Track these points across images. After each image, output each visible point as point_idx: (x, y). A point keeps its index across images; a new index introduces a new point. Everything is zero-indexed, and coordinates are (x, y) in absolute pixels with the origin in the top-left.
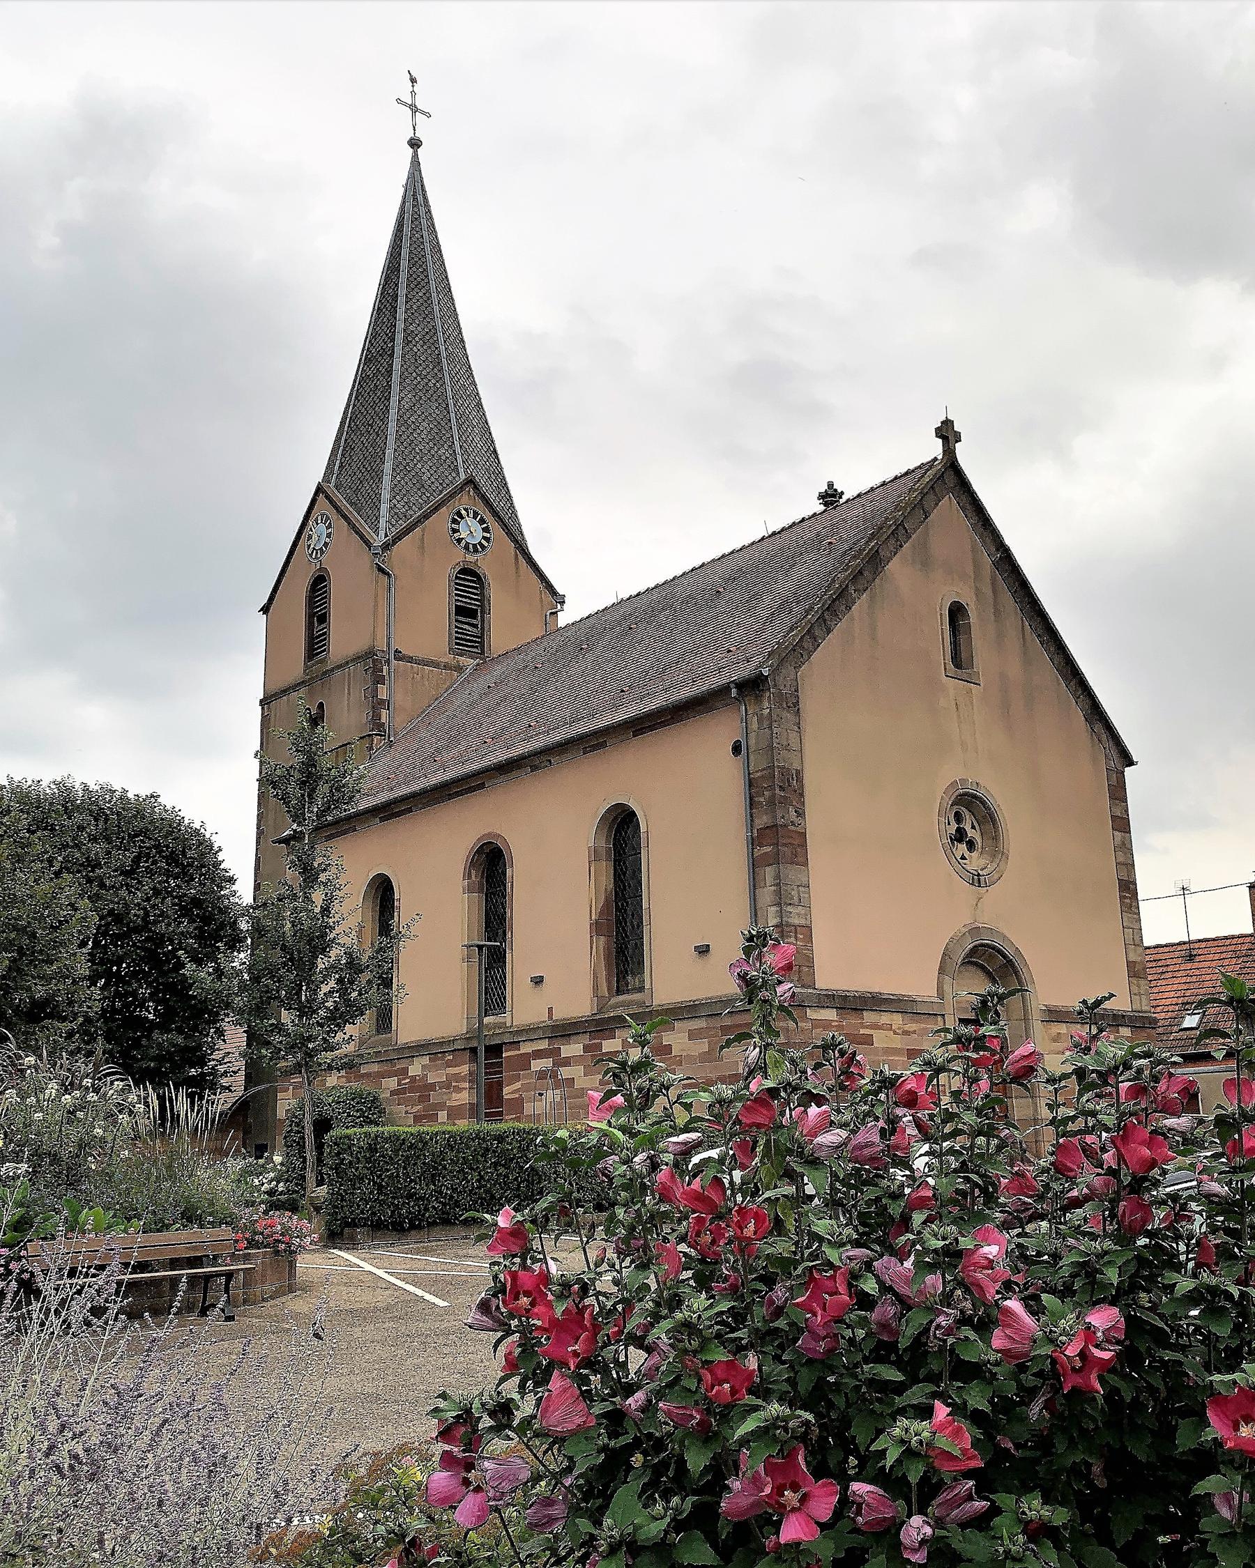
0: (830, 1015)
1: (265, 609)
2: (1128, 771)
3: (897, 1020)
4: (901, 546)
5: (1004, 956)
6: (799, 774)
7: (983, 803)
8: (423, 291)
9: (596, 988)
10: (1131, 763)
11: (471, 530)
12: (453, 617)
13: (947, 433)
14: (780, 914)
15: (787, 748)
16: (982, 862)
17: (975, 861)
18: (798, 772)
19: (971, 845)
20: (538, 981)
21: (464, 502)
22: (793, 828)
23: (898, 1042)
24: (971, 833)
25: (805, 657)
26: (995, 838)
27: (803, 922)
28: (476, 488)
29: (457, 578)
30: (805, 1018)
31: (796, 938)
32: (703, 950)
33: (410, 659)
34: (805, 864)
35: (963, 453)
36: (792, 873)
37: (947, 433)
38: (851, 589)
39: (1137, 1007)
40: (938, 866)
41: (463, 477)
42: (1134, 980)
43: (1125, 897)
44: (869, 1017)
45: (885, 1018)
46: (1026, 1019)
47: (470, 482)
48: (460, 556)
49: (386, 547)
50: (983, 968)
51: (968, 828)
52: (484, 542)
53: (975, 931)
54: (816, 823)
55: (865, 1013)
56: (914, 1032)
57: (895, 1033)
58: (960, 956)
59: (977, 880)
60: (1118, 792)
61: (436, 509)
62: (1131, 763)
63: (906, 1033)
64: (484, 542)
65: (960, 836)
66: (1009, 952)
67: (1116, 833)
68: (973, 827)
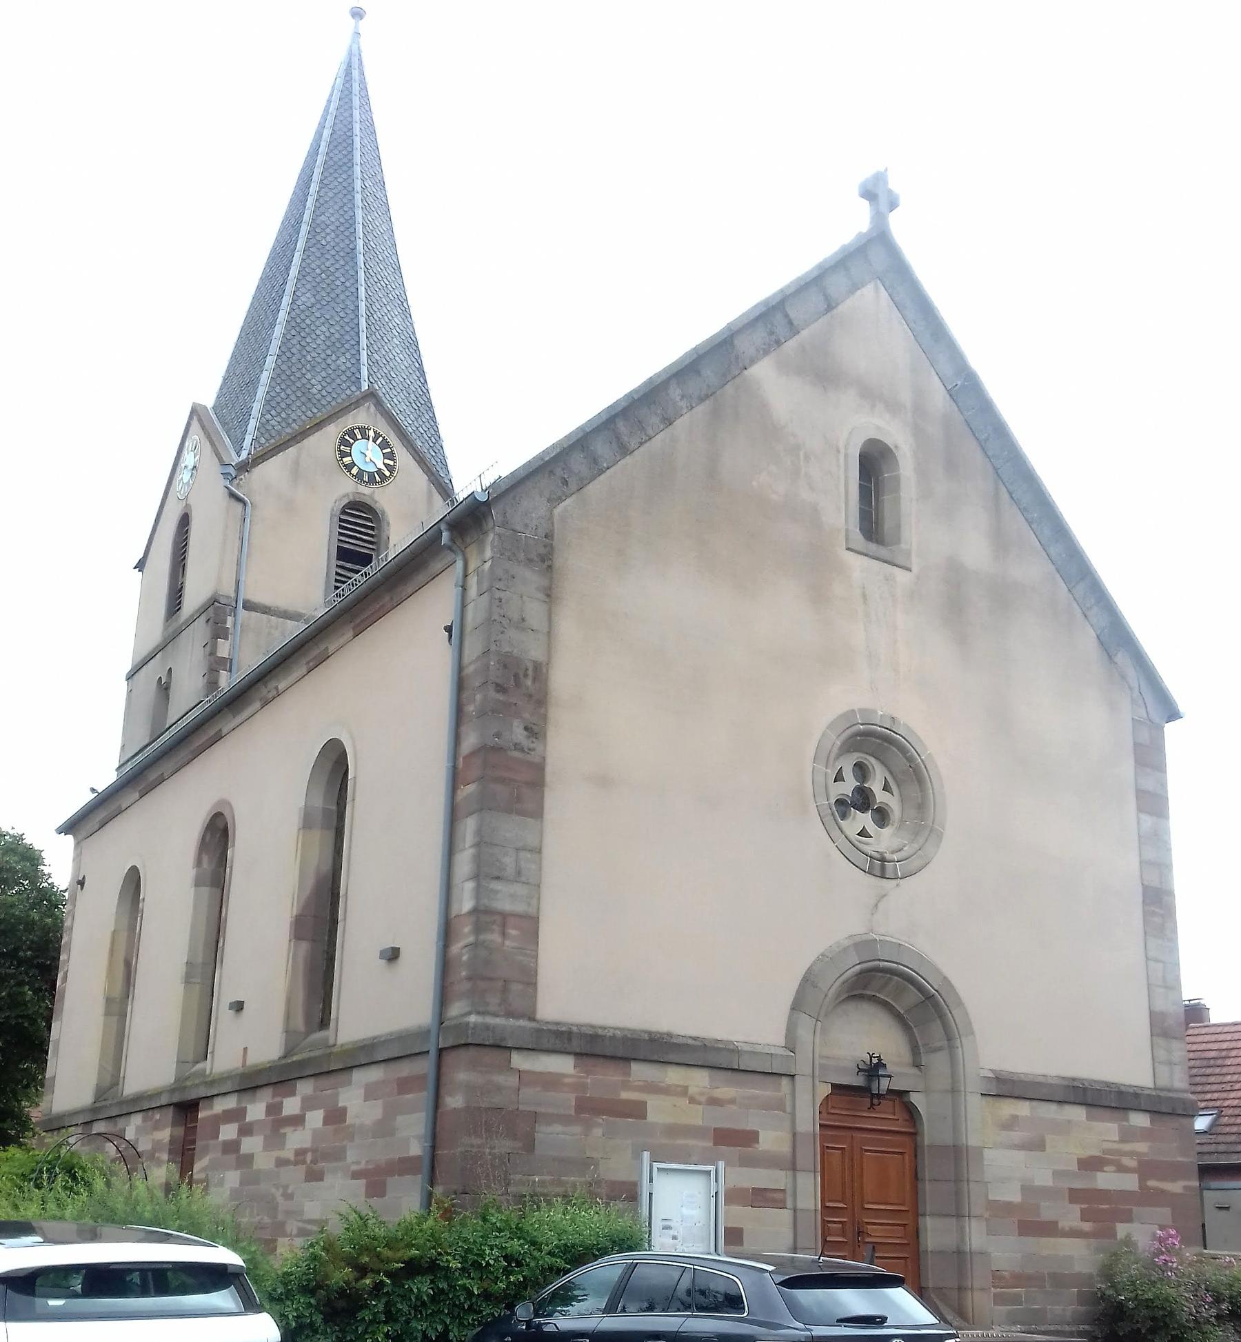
0: (562, 1065)
1: (140, 566)
2: (1170, 729)
3: (698, 1080)
4: (778, 343)
5: (920, 989)
6: (540, 672)
7: (903, 750)
8: (344, 176)
9: (288, 1017)
10: (1173, 714)
11: (368, 455)
12: (334, 562)
13: (876, 194)
14: (478, 893)
15: (521, 623)
16: (896, 843)
17: (884, 840)
18: (537, 667)
19: (882, 817)
20: (238, 1007)
21: (361, 417)
22: (517, 754)
23: (696, 1116)
24: (881, 797)
25: (573, 486)
26: (921, 807)
27: (520, 908)
28: (379, 404)
29: (343, 512)
30: (507, 1068)
31: (504, 934)
32: (393, 955)
33: (266, 610)
34: (538, 814)
35: (898, 225)
36: (509, 828)
37: (876, 194)
38: (675, 392)
39: (1163, 1082)
40: (813, 844)
41: (365, 386)
42: (1161, 1041)
43: (1154, 913)
44: (639, 1071)
45: (674, 1076)
46: (954, 1091)
47: (372, 395)
48: (347, 488)
49: (244, 467)
50: (885, 1005)
51: (876, 786)
52: (347, 449)
53: (864, 945)
54: (563, 749)
55: (635, 1067)
56: (732, 1101)
57: (692, 1100)
58: (831, 983)
59: (879, 867)
60: (1149, 756)
61: (319, 425)
62: (1173, 714)
63: (714, 1102)
64: (347, 449)
65: (863, 800)
66: (932, 984)
67: (1144, 817)
68: (886, 788)
